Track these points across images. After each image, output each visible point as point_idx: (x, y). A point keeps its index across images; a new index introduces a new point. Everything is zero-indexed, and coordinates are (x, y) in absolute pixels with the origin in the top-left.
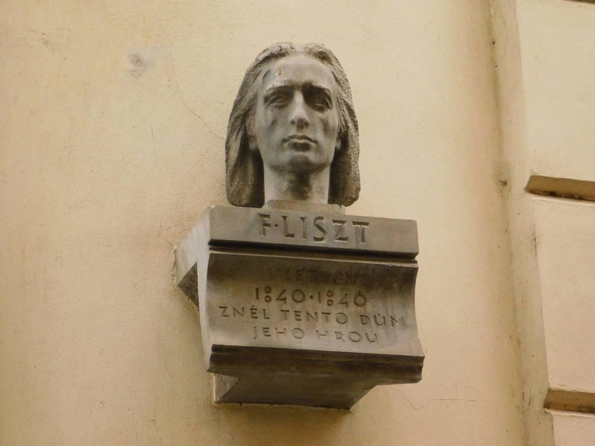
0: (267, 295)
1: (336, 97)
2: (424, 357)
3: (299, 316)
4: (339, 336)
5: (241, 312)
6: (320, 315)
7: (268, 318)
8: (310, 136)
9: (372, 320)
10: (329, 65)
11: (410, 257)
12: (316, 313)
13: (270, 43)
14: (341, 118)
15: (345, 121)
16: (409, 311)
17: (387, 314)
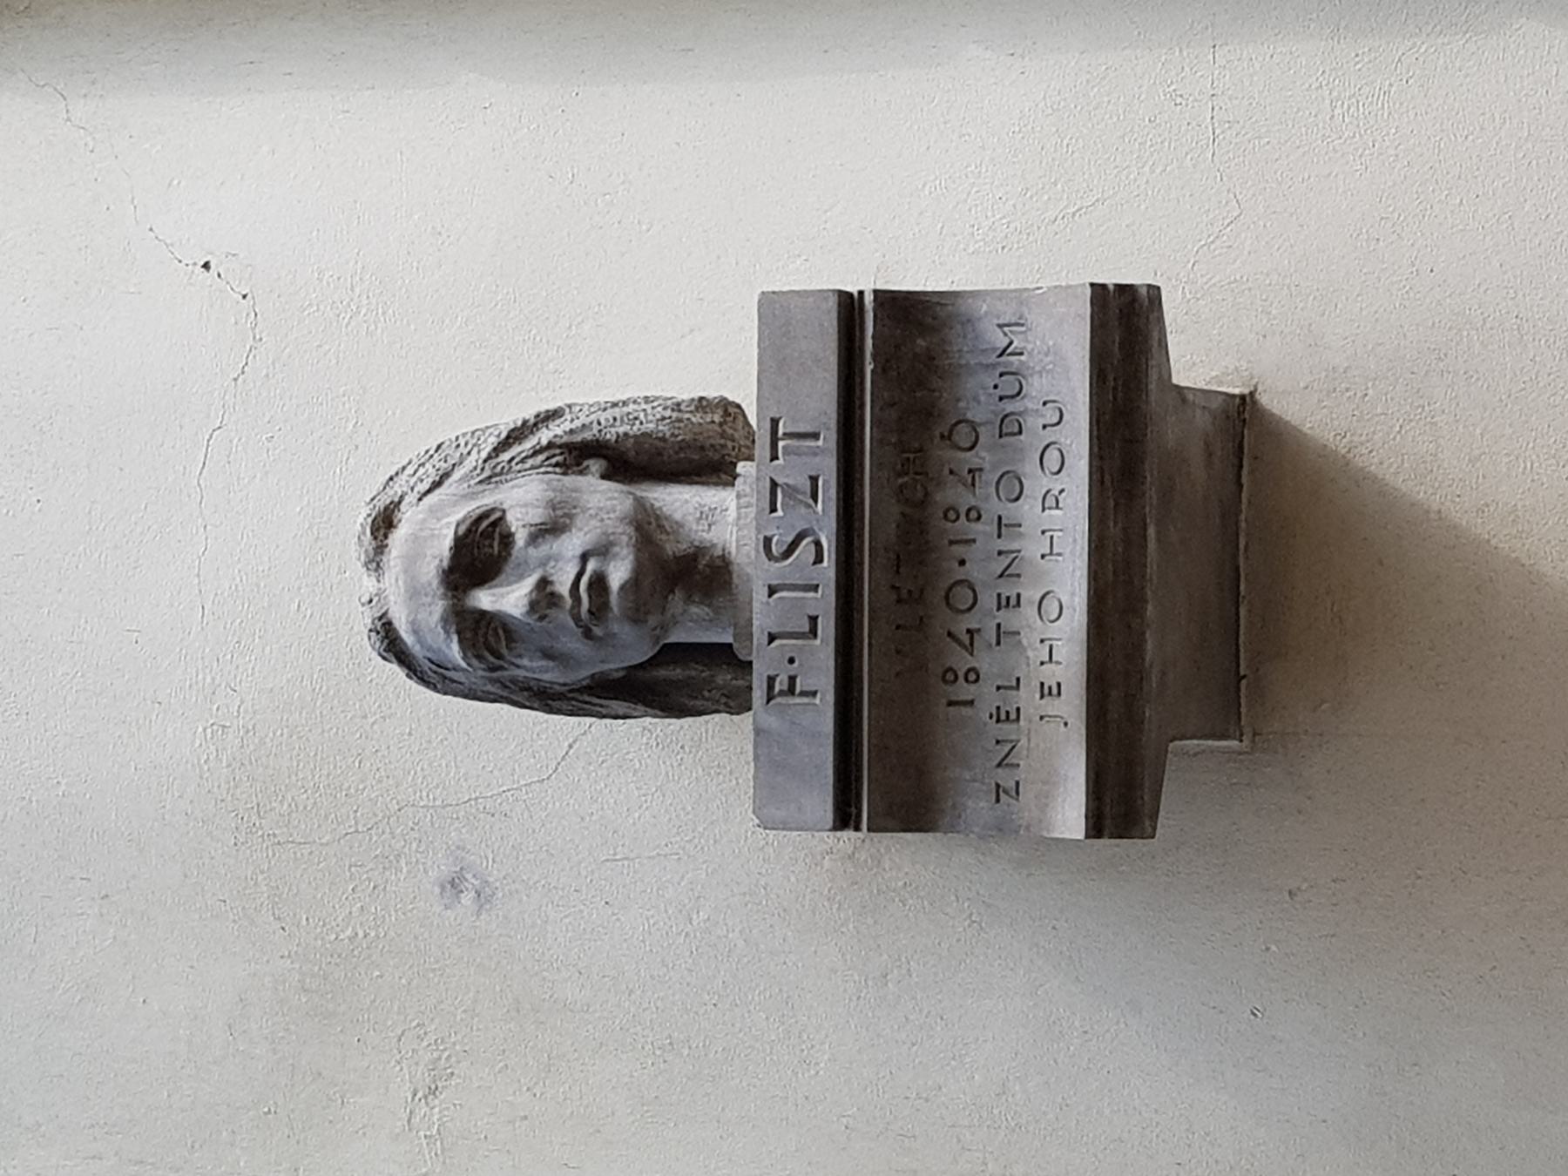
0: (963, 517)
1: (481, 488)
2: (1092, 285)
3: (1008, 598)
4: (1050, 501)
5: (1008, 747)
6: (1002, 544)
7: (1018, 680)
8: (571, 571)
9: (1009, 407)
10: (403, 507)
11: (849, 305)
12: (1000, 553)
13: (368, 651)
14: (527, 466)
15: (535, 453)
16: (985, 308)
17: (994, 366)
